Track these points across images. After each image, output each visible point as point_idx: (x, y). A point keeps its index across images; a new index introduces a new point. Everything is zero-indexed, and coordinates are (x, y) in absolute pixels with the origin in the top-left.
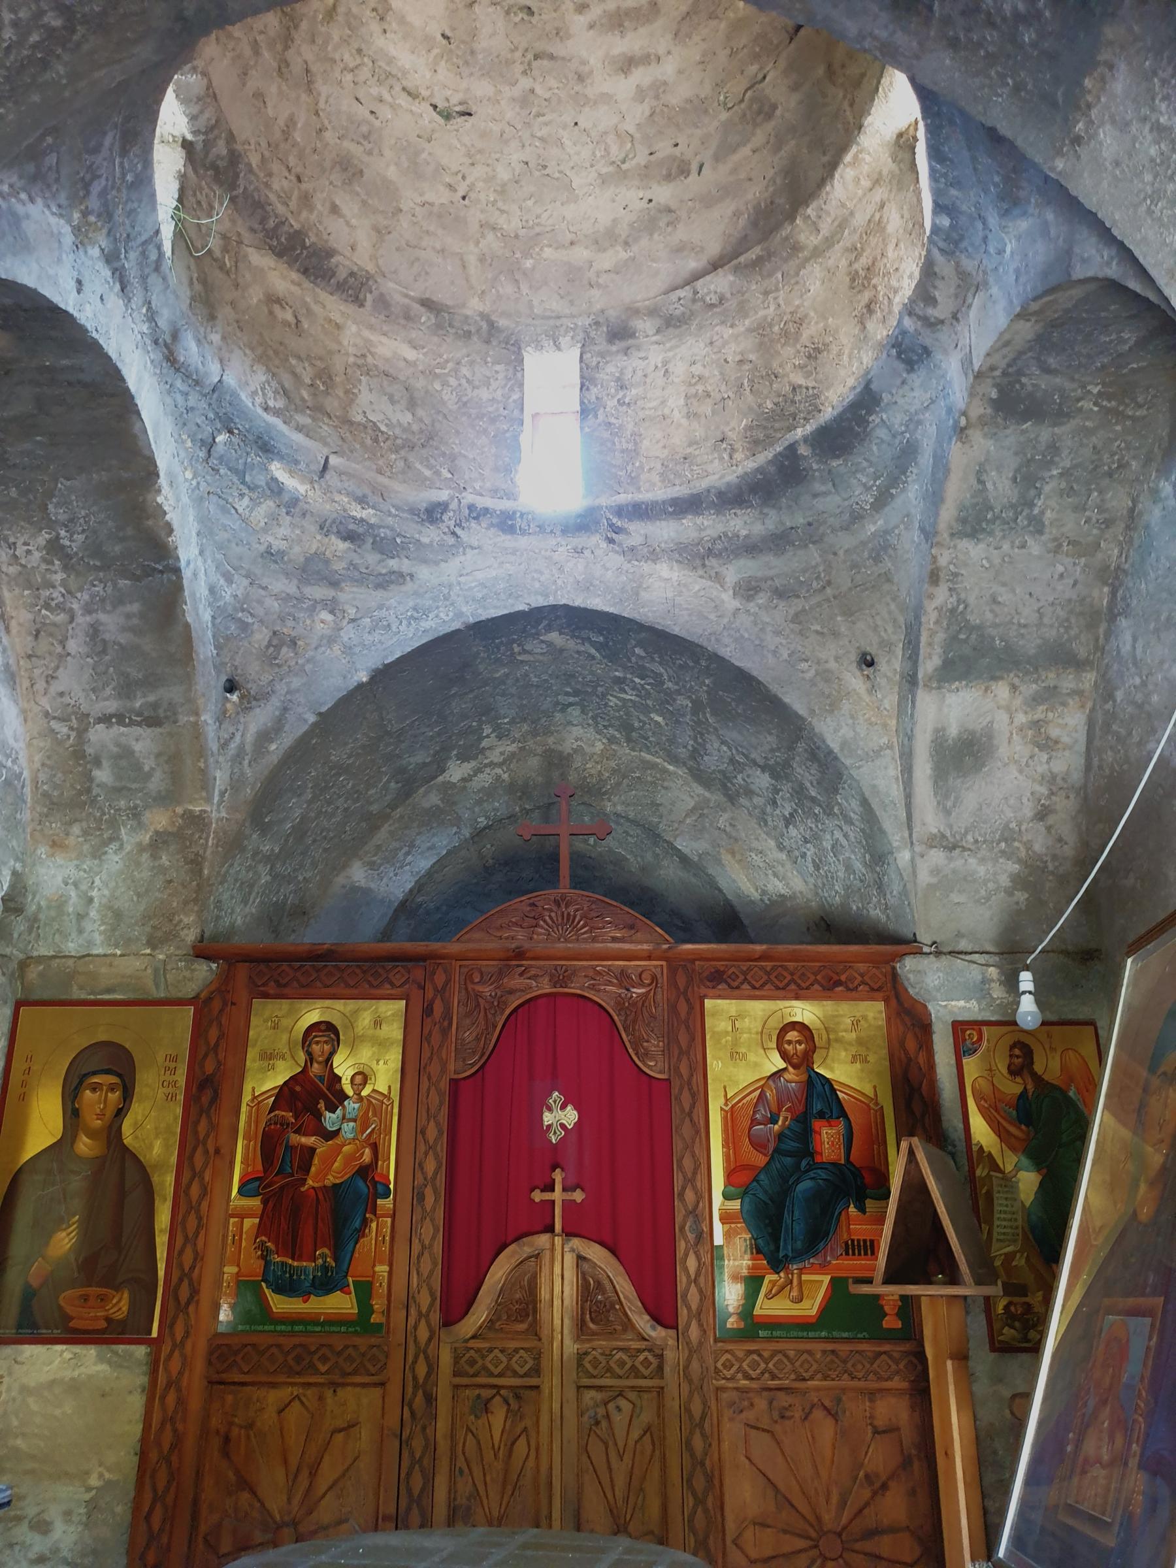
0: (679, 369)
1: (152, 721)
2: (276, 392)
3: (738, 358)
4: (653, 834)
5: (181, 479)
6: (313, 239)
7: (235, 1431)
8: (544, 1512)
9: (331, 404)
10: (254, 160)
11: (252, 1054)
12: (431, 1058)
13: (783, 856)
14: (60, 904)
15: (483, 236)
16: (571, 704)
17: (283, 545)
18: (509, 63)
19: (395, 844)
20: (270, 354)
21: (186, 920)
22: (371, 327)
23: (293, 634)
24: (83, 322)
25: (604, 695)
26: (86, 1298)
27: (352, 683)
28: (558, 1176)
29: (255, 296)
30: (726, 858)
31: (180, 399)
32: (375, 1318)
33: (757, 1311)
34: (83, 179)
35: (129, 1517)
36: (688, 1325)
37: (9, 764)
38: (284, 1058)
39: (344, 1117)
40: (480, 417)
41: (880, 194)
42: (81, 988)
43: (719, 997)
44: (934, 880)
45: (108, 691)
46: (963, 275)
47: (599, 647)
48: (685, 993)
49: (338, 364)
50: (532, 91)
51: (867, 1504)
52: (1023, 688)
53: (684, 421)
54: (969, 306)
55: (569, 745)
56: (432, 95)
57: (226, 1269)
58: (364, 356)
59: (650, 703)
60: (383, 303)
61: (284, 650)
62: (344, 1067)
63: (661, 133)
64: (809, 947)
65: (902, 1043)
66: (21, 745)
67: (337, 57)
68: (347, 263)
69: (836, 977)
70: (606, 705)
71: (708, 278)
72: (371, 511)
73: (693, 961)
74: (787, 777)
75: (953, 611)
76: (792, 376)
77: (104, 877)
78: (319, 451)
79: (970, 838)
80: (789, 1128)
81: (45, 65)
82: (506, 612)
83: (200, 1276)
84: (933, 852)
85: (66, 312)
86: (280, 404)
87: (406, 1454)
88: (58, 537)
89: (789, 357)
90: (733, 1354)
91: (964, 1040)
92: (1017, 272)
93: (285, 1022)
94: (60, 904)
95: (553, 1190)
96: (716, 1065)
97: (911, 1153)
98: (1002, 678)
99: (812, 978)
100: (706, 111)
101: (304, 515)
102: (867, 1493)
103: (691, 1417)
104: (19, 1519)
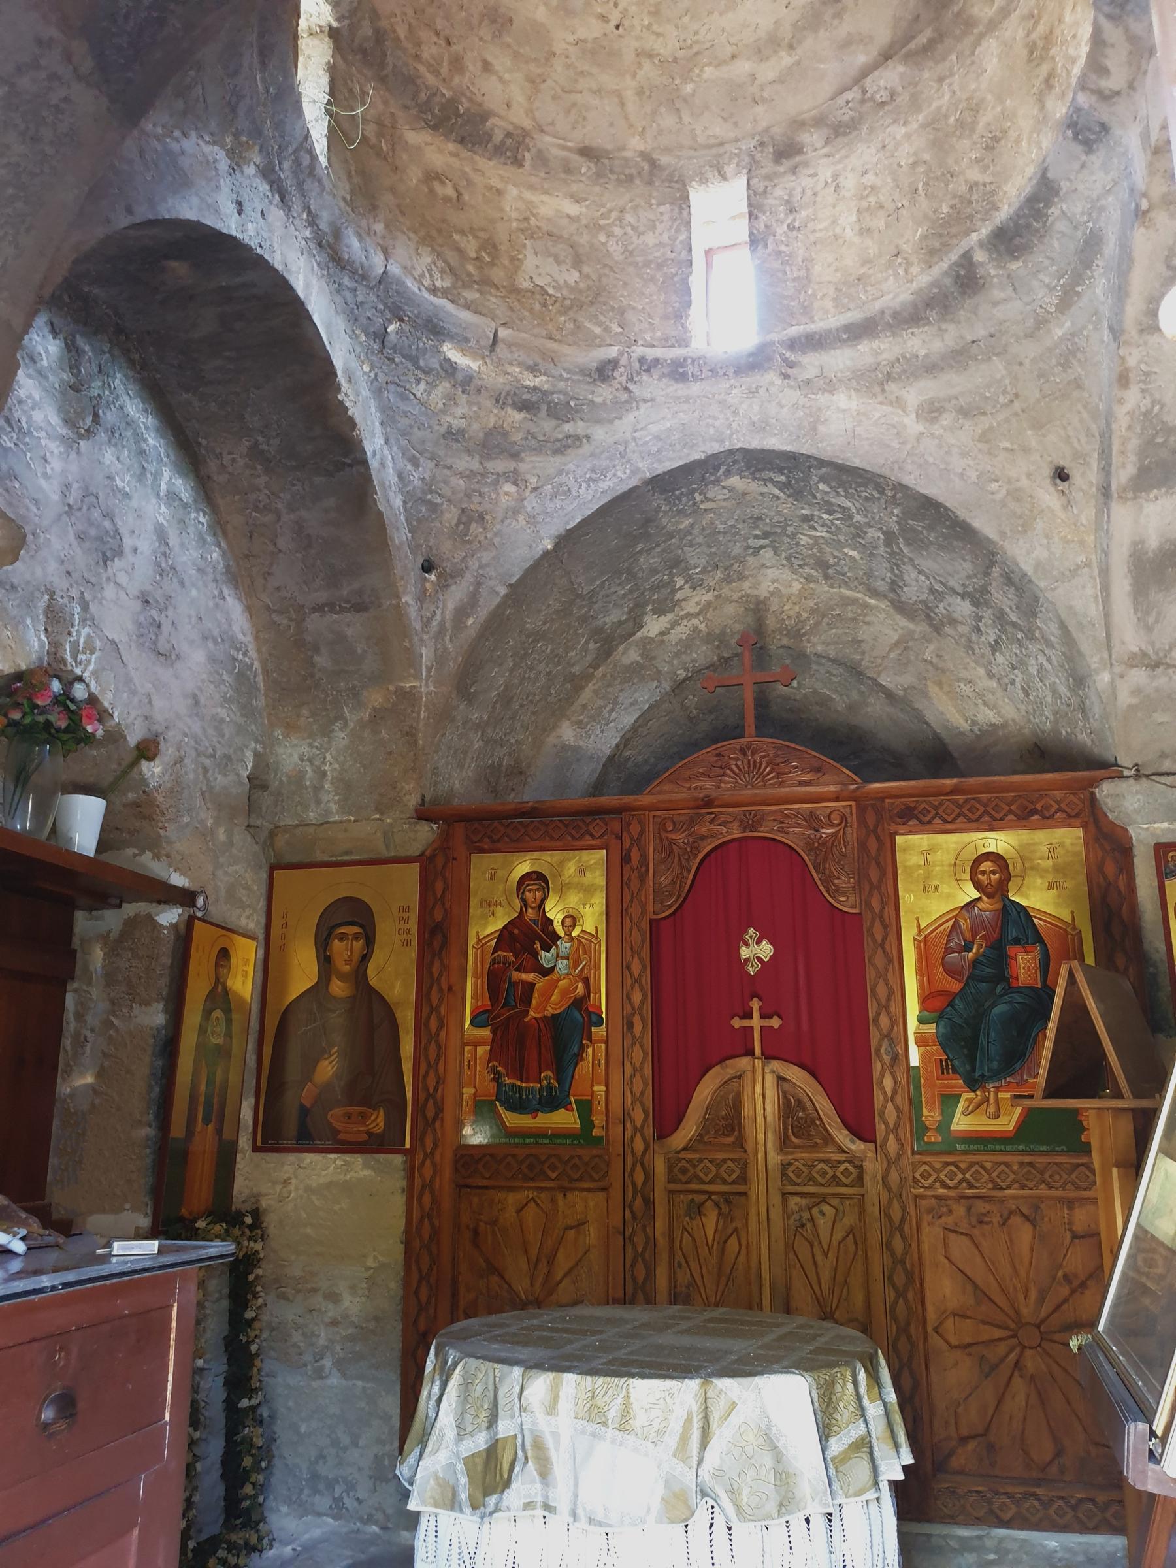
0: (850, 182)
1: (360, 608)
2: (442, 272)
3: (911, 161)
4: (855, 671)
5: (359, 373)
6: (466, 104)
10: (402, 32)
11: (474, 902)
12: (631, 901)
13: (993, 684)
14: (298, 778)
15: (640, 65)
16: (762, 547)
17: (462, 423)
19: (601, 703)
22: (531, 187)
23: (481, 509)
24: (247, 241)
25: (794, 535)
28: (755, 1004)
29: (414, 176)
30: (933, 690)
31: (348, 294)
32: (596, 1132)
33: (954, 1126)
34: (229, 103)
35: (401, 1292)
36: (885, 1140)
37: (241, 657)
38: (502, 905)
40: (647, 264)
43: (911, 833)
44: (1134, 701)
46: (1133, 39)
47: (782, 486)
48: (875, 831)
49: (502, 234)
51: (1066, 1300)
53: (857, 240)
54: (1145, 73)
55: (763, 591)
57: (464, 1090)
58: (526, 219)
59: (842, 538)
60: (542, 159)
61: (473, 525)
62: (555, 911)
64: (1002, 778)
65: (1101, 868)
68: (502, 123)
70: (797, 544)
71: (876, 73)
72: (544, 378)
73: (882, 799)
74: (987, 604)
75: (1145, 414)
78: (486, 326)
82: (682, 463)
83: (443, 1096)
84: (1134, 671)
85: (230, 236)
88: (256, 443)
93: (501, 873)
94: (301, 775)
96: (907, 899)
97: (1071, 975)
101: (479, 391)
102: (1065, 1291)
103: (891, 1220)
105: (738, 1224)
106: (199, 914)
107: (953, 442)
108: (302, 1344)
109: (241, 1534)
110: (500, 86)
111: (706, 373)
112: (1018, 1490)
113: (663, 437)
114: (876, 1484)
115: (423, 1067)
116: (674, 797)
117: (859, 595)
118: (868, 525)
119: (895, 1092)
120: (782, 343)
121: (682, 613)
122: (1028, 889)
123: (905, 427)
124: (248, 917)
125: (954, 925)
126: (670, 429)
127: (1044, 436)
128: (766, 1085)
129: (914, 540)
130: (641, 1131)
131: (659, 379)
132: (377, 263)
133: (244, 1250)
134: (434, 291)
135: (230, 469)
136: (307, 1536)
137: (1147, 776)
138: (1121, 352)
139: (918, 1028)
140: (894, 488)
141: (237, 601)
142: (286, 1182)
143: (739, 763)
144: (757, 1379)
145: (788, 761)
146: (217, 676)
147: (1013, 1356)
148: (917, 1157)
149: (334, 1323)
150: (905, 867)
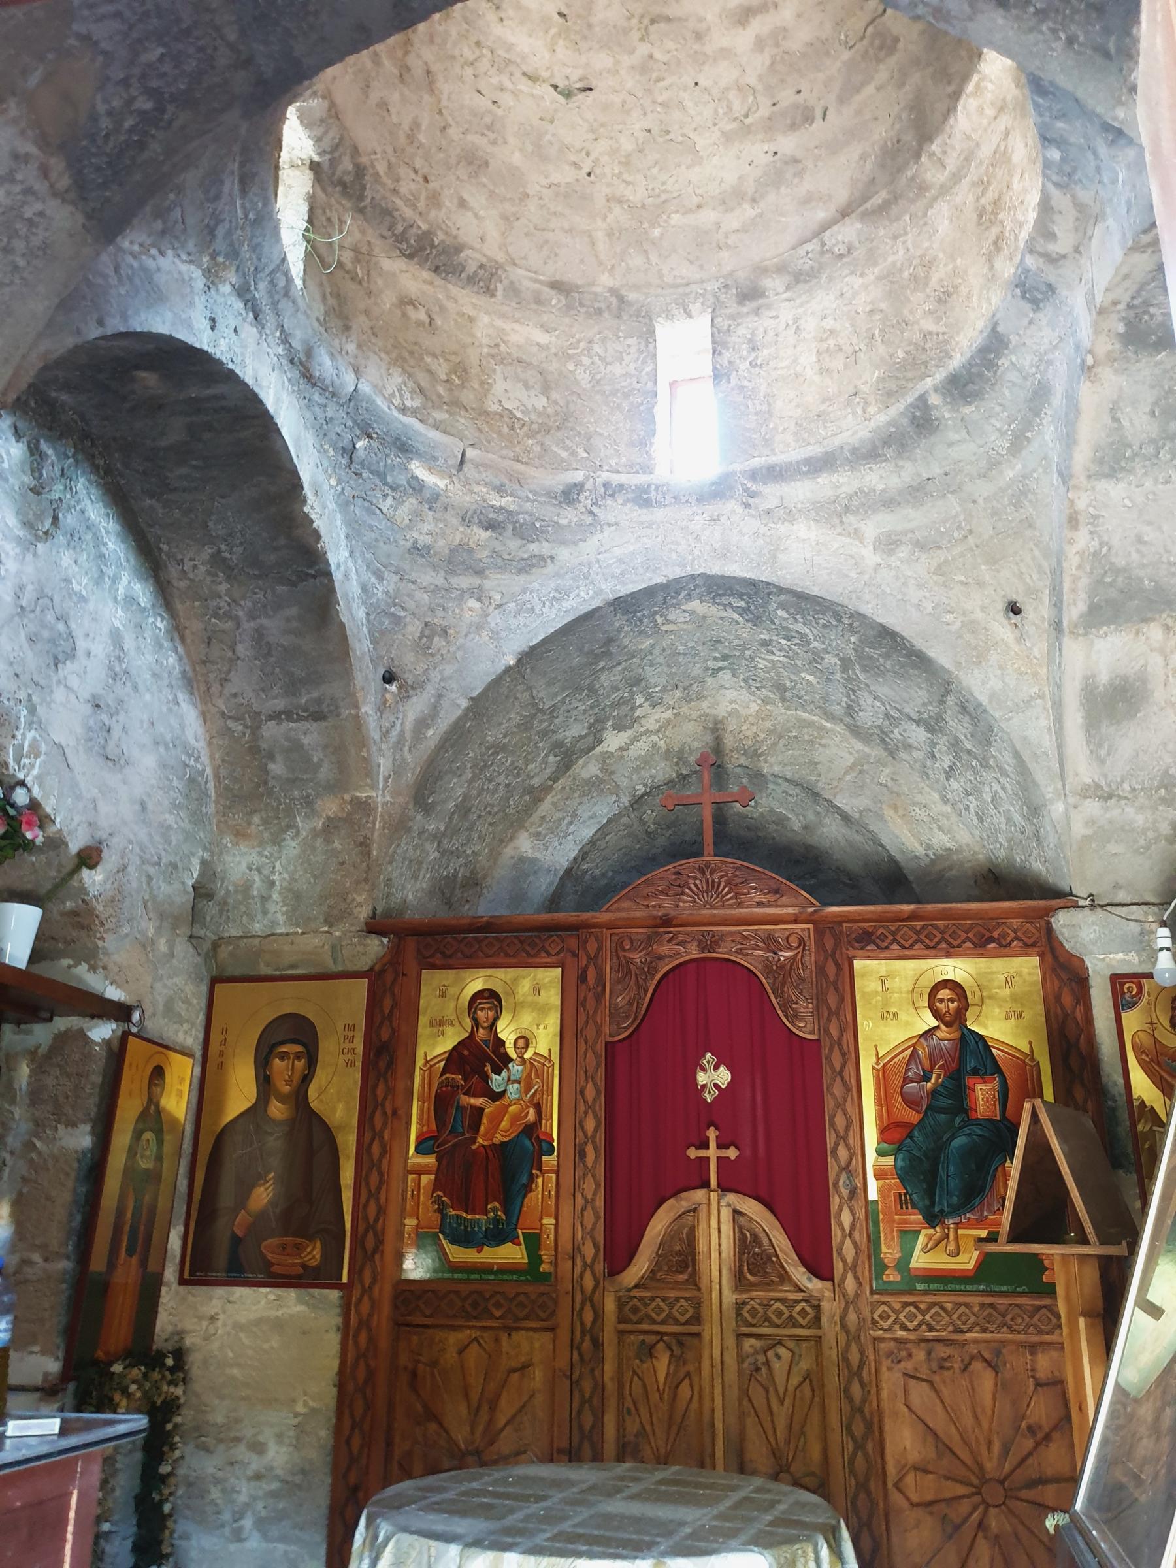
0: (810, 325)
1: (318, 717)
2: (412, 392)
4: (813, 794)
5: (326, 487)
7: (421, 1367)
8: (709, 1451)
9: (467, 397)
10: (381, 168)
11: (423, 1020)
12: (587, 1022)
13: (948, 809)
14: (247, 887)
16: (721, 669)
18: (626, 31)
19: (559, 815)
20: (405, 356)
21: (358, 899)
22: (503, 316)
26: (284, 1247)
27: (500, 668)
28: (712, 1134)
29: (388, 300)
30: (888, 813)
31: (317, 409)
32: (544, 1268)
33: (914, 1264)
36: (843, 1279)
40: (614, 393)
41: (1005, 121)
42: (268, 965)
43: (869, 958)
44: (1089, 832)
45: (276, 690)
46: (1080, 207)
47: (743, 612)
49: (473, 357)
50: (651, 56)
51: (1030, 1454)
53: (817, 379)
54: (1091, 238)
55: (721, 711)
56: (552, 76)
57: (407, 1222)
58: (497, 345)
59: (799, 663)
60: (513, 290)
61: (436, 639)
62: (507, 1032)
63: (782, 81)
67: (457, 53)
68: (477, 256)
69: (988, 934)
71: (835, 228)
72: (510, 499)
73: (840, 923)
74: (941, 730)
75: (1095, 554)
76: (922, 322)
77: (284, 862)
79: (1126, 786)
81: (142, 146)
82: (644, 586)
86: (417, 403)
87: (576, 1394)
88: (219, 551)
89: (919, 304)
90: (890, 1307)
92: (1129, 203)
93: (452, 991)
94: (247, 887)
95: (707, 1147)
96: (866, 1025)
97: (1034, 1115)
98: (1153, 620)
99: (964, 935)
100: (827, 53)
102: (1029, 1444)
104: (238, 1440)
105: (691, 1367)
106: (134, 1030)
110: (475, 221)
117: (816, 718)
118: (826, 651)
119: (853, 1227)
129: (869, 666)
130: (591, 1267)
132: (348, 380)
134: (403, 410)
135: (191, 576)
140: (851, 616)
142: (213, 1319)
145: (746, 882)
147: (976, 1516)
149: (258, 1477)
150: (864, 994)
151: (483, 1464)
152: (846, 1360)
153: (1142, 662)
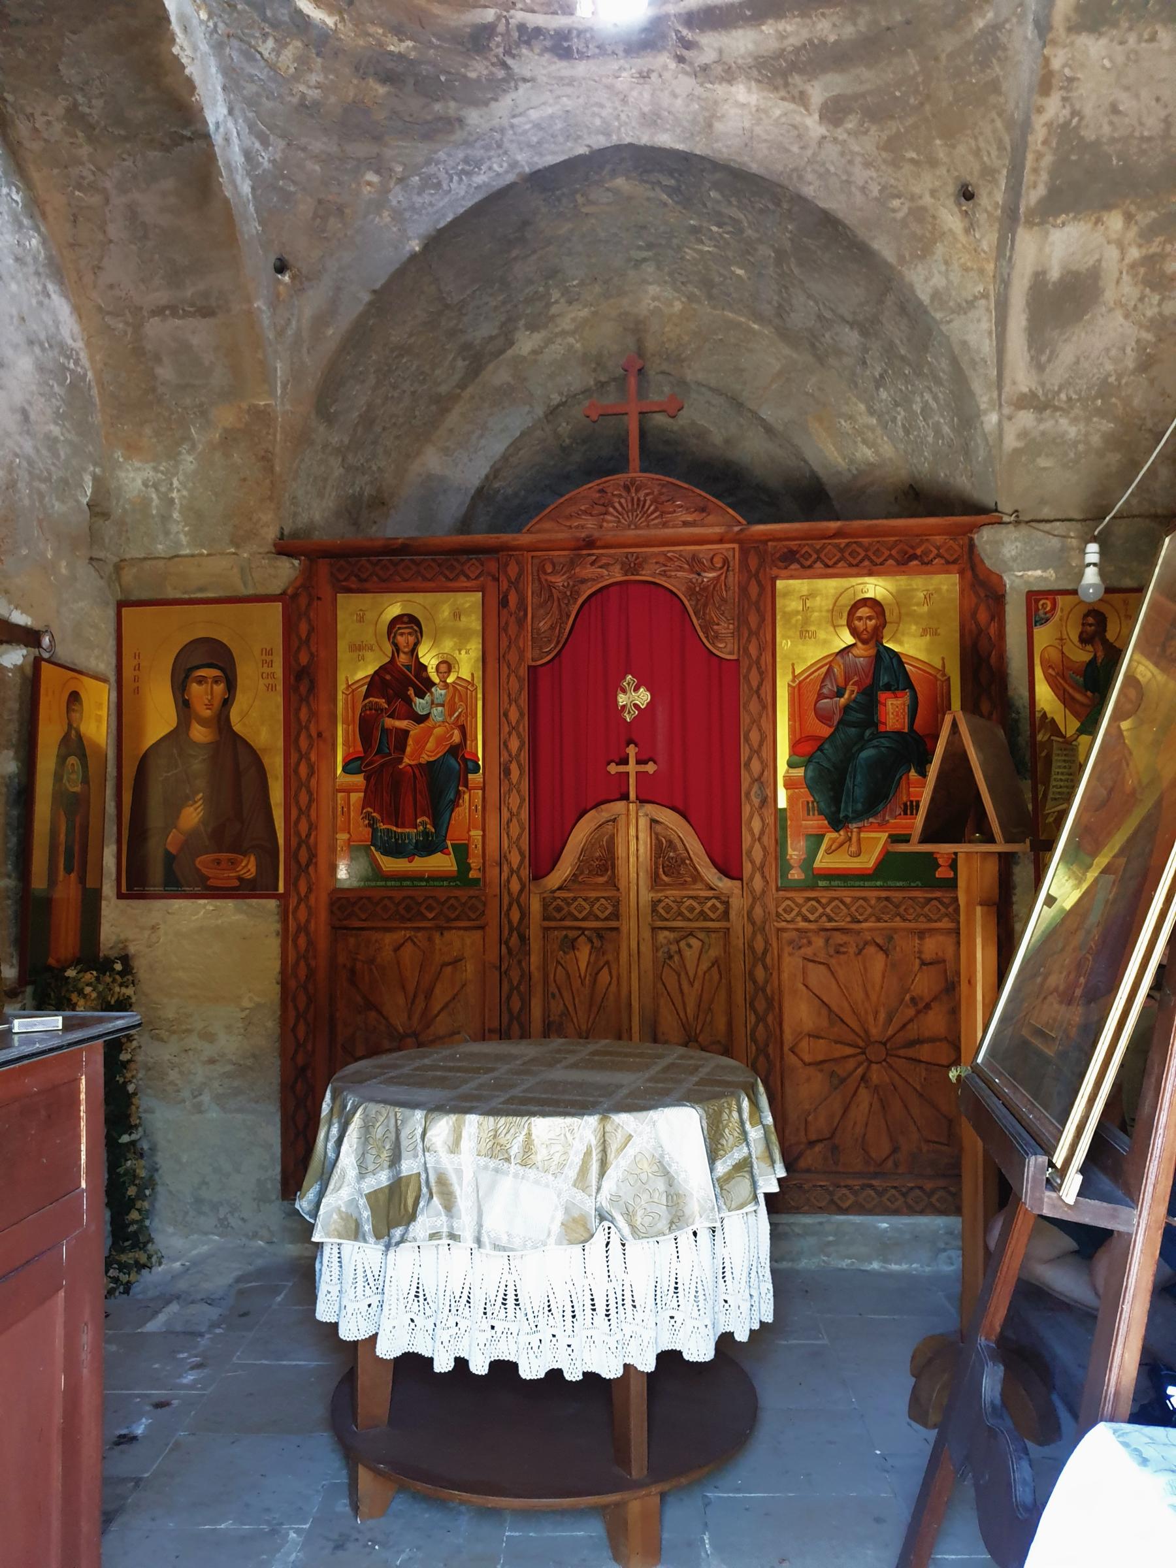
1: (206, 312)
4: (737, 404)
5: (195, 22)
11: (342, 646)
12: (509, 647)
16: (645, 260)
25: (679, 248)
28: (632, 751)
32: (472, 874)
33: (817, 864)
36: (752, 878)
37: (72, 366)
39: (432, 702)
44: (1019, 444)
47: (673, 191)
48: (756, 575)
51: (911, 1020)
52: (1139, 217)
57: (339, 836)
59: (730, 254)
61: (332, 220)
62: (429, 657)
64: (885, 522)
65: (974, 614)
66: (79, 345)
69: (911, 552)
70: (682, 258)
72: (410, 43)
73: (766, 542)
75: (1065, 125)
77: (181, 478)
79: (1063, 396)
80: (854, 701)
82: (566, 157)
83: (316, 843)
88: (76, 104)
91: (1037, 609)
93: (369, 616)
94: (145, 502)
95: (627, 763)
96: (784, 645)
97: (954, 725)
99: (887, 553)
102: (911, 1012)
104: (189, 1031)
105: (610, 957)
106: (46, 655)
107: (857, 149)
108: (178, 1082)
109: (131, 1255)
111: (593, 50)
112: (856, 1183)
113: (544, 125)
114: (755, 1197)
115: (294, 813)
116: (554, 536)
117: (743, 319)
118: (760, 241)
119: (762, 832)
120: (678, 16)
121: (557, 330)
122: (903, 634)
123: (807, 128)
124: (97, 658)
125: (828, 670)
126: (551, 117)
127: (954, 147)
128: (640, 827)
130: (518, 872)
131: (541, 55)
133: (116, 997)
135: (45, 135)
136: (194, 1252)
137: (1027, 522)
138: (1046, 51)
139: (787, 772)
141: (63, 300)
142: (154, 928)
143: (623, 501)
144: (651, 1113)
145: (672, 500)
146: (47, 388)
147: (860, 1071)
148: (781, 893)
149: (212, 1061)
150: (785, 613)
151: (420, 1045)
152: (751, 948)
153: (1097, 257)
